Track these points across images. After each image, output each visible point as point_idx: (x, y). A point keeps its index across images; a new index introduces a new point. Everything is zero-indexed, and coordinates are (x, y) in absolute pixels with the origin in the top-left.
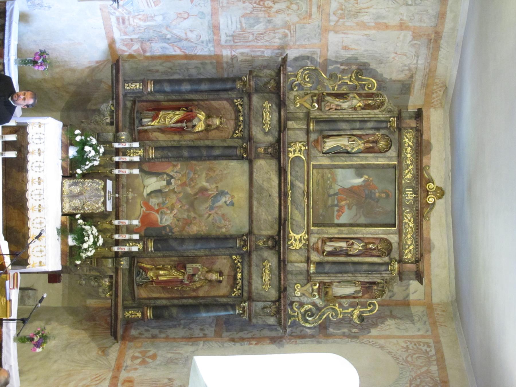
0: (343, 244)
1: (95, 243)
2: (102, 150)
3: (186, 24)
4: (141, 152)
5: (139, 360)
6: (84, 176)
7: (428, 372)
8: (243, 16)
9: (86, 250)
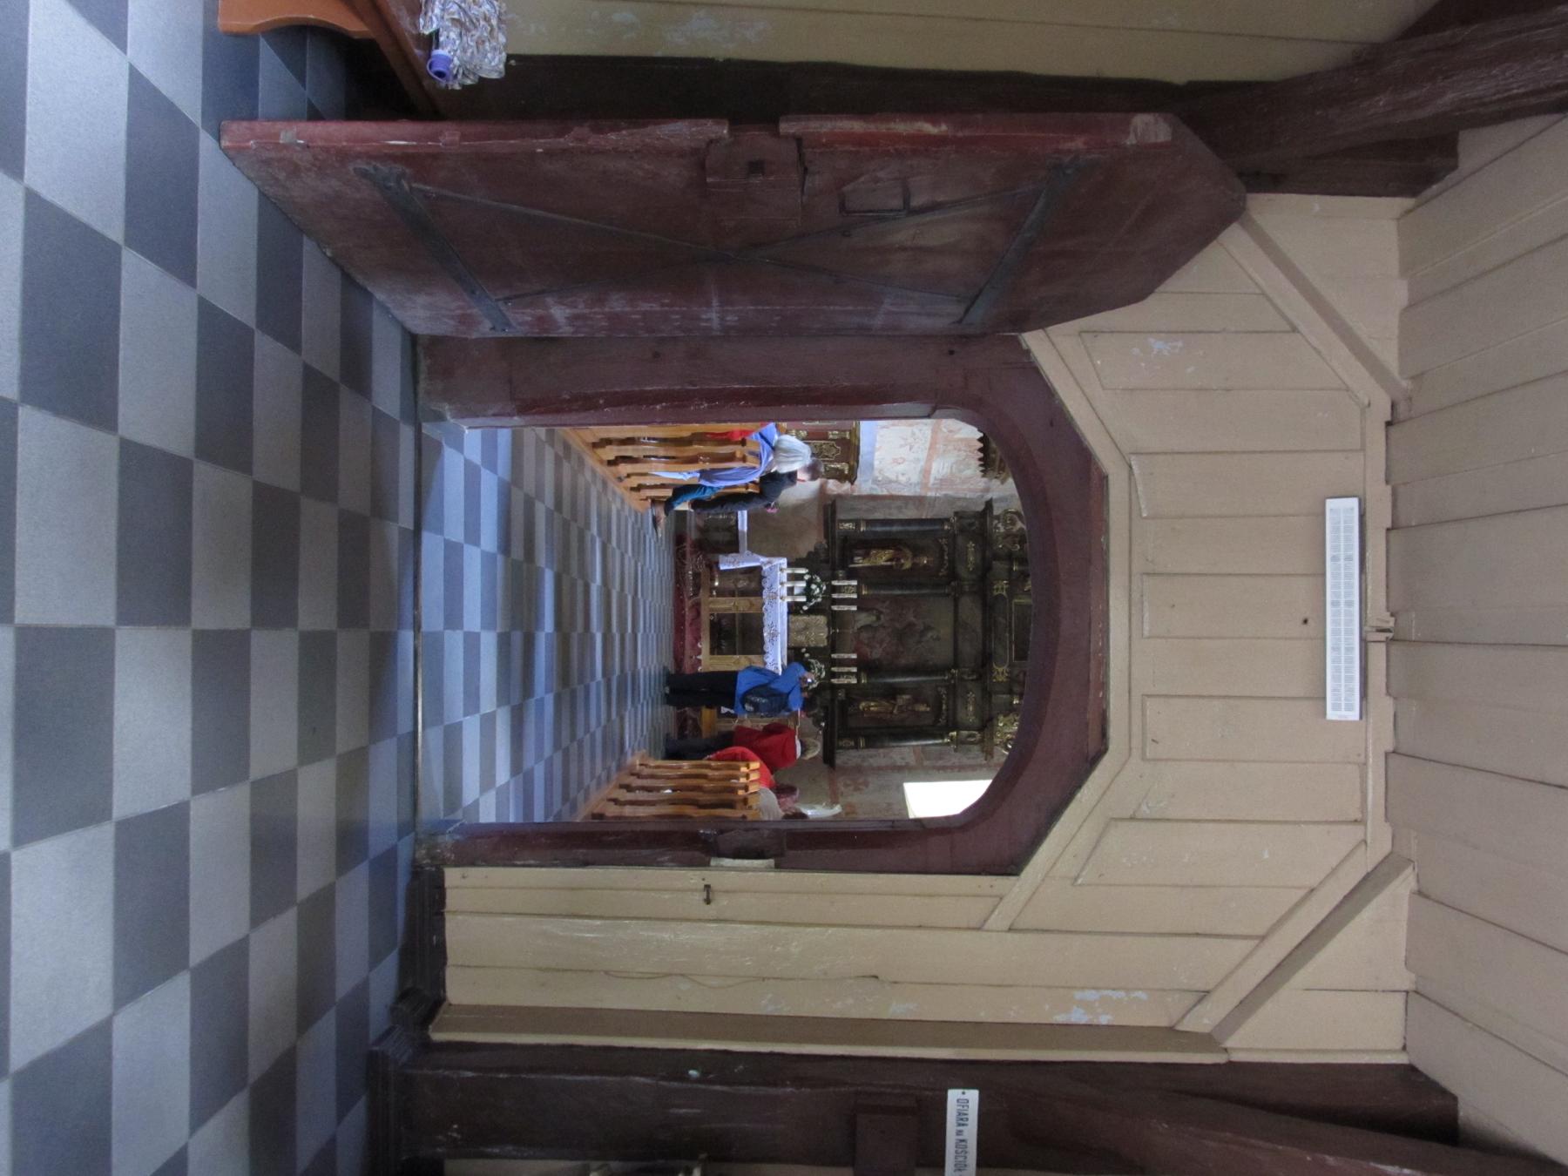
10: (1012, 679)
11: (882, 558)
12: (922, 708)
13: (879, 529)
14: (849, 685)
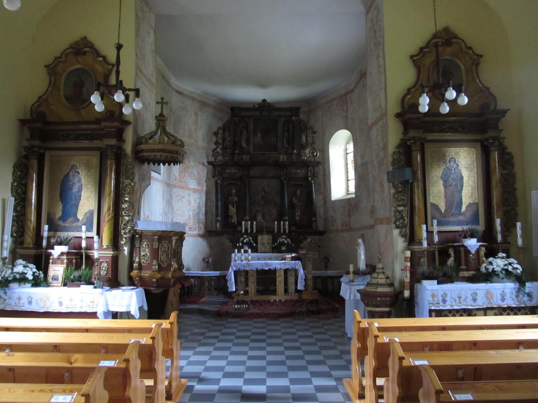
0: (285, 140)
3: (193, 202)
6: (257, 244)
8: (190, 178)
9: (288, 242)
11: (233, 210)
12: (298, 192)
13: (220, 211)
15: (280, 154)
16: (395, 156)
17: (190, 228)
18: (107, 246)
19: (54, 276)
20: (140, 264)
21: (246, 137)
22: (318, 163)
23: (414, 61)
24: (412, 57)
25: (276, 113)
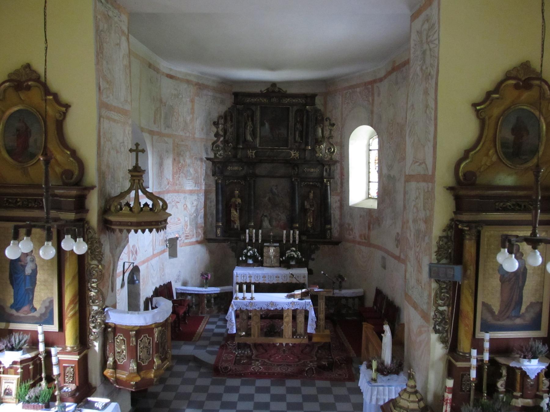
1: (294, 251)
2: (250, 247)
3: (189, 206)
4: (251, 229)
5: (351, 232)
6: (262, 256)
7: (360, 93)
10: (298, 149)
11: (235, 214)
12: (311, 195)
13: (220, 216)
14: (299, 235)
15: (291, 149)
16: (441, 243)
17: (187, 236)
18: (71, 348)
19: (6, 390)
20: (115, 362)
21: (251, 129)
22: (336, 162)
23: (477, 111)
24: (474, 105)
25: (286, 101)
